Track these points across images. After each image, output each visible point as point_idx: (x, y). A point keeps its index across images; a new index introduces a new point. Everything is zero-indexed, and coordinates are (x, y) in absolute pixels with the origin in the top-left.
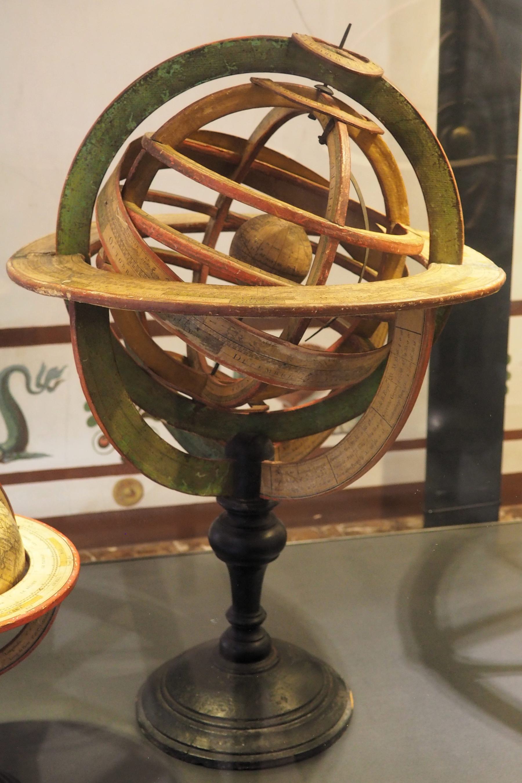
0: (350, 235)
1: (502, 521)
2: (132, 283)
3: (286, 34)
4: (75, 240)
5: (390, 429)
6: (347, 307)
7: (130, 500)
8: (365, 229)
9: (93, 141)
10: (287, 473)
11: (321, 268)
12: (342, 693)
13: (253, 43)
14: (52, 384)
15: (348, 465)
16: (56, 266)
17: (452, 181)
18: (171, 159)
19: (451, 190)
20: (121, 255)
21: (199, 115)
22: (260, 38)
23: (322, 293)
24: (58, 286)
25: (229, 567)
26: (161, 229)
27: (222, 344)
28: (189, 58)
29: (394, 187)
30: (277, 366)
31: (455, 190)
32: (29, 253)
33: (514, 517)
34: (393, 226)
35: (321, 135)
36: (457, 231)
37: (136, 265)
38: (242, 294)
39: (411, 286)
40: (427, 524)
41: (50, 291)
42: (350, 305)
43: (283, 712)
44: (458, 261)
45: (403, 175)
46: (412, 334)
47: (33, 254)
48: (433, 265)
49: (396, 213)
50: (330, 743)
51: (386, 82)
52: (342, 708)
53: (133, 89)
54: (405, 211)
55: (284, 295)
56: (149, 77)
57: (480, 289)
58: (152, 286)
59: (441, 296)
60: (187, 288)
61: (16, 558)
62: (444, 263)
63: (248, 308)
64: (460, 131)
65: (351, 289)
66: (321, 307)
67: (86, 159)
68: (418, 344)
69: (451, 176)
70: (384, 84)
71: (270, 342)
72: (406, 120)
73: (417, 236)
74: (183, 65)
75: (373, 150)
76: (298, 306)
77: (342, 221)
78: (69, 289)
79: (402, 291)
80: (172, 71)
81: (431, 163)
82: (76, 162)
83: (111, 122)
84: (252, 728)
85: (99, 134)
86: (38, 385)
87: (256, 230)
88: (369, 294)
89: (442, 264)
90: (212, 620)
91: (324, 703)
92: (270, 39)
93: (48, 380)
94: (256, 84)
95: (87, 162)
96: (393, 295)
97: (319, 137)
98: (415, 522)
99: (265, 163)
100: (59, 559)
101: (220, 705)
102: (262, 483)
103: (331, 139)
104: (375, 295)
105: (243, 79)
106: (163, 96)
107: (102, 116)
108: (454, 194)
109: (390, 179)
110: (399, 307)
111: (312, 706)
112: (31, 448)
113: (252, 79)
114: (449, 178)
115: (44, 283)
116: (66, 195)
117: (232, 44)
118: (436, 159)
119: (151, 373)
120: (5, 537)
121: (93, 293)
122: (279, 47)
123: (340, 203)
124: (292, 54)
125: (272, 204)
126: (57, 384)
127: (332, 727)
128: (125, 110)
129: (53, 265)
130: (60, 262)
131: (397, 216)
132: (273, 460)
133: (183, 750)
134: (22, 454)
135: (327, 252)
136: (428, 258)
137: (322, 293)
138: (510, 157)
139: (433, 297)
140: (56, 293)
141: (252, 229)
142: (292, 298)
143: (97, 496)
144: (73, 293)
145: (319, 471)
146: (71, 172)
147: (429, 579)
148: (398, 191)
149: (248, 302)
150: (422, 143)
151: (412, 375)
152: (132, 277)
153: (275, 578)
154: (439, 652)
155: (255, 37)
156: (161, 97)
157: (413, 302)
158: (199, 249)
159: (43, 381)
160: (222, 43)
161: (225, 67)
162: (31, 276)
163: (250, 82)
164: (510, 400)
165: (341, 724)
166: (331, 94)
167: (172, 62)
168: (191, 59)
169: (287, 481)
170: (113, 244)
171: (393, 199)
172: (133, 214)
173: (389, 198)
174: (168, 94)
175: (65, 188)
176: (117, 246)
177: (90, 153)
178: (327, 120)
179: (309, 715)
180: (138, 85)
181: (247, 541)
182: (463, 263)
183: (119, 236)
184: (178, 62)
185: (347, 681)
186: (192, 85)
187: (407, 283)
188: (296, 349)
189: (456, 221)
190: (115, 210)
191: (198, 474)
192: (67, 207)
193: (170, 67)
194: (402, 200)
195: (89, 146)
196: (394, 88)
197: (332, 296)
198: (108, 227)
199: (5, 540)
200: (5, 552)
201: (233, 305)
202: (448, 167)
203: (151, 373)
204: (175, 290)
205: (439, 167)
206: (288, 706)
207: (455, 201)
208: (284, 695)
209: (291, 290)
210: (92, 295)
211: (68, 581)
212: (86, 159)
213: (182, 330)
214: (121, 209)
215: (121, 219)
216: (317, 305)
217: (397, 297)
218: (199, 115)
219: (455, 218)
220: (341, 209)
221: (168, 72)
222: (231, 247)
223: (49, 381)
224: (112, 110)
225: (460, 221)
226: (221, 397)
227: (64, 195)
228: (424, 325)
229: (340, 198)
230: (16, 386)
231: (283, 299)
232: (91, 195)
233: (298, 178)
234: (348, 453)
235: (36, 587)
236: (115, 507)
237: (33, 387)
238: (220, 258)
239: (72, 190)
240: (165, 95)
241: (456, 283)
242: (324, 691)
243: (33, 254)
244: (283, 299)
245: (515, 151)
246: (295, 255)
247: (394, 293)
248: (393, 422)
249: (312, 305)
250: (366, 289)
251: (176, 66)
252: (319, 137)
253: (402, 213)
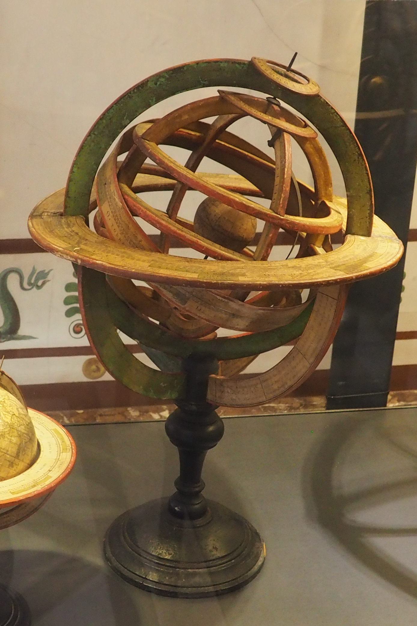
0: (288, 223)
1: (390, 405)
2: (124, 252)
3: (247, 58)
4: (78, 202)
5: (308, 366)
6: (284, 284)
7: (96, 374)
8: (299, 216)
9: (96, 133)
10: (228, 387)
11: (265, 247)
12: (258, 544)
13: (222, 65)
14: (40, 283)
15: (275, 387)
16: (66, 229)
17: (368, 174)
18: (157, 158)
19: (366, 180)
20: (116, 226)
21: (178, 120)
22: (227, 61)
23: (266, 269)
24: (71, 253)
25: (179, 451)
26: (148, 212)
27: (188, 299)
28: (172, 73)
29: (322, 173)
30: (228, 316)
31: (369, 181)
32: (43, 212)
33: (399, 401)
34: (320, 202)
35: (270, 139)
36: (369, 212)
37: (127, 236)
38: (207, 269)
39: (332, 264)
40: (329, 406)
41: (65, 256)
42: (286, 283)
43: (214, 558)
44: (368, 233)
45: (331, 170)
46: (330, 299)
47: (46, 214)
48: (349, 237)
49: (322, 192)
50: (246, 582)
51: (321, 97)
52: (257, 557)
54: (330, 191)
55: (238, 271)
56: (141, 87)
57: (382, 267)
58: (140, 257)
59: (353, 275)
60: (165, 260)
61: (33, 446)
62: (357, 235)
63: (212, 283)
64: (376, 80)
65: (287, 265)
66: (265, 284)
67: (90, 146)
68: (334, 307)
69: (367, 171)
70: (320, 100)
71: (224, 300)
72: (336, 127)
73: (338, 214)
74: (167, 79)
75: (308, 146)
76: (248, 282)
77: (282, 211)
78: (80, 257)
79: (325, 269)
80: (158, 83)
82: (82, 148)
83: (110, 119)
84: (191, 569)
85: (101, 127)
86: (30, 284)
87: (217, 206)
88: (300, 272)
89: (356, 236)
90: (176, 508)
91: (244, 552)
93: (37, 280)
94: (223, 98)
96: (318, 274)
97: (268, 141)
98: (319, 401)
99: (223, 143)
100: (61, 446)
101: (167, 550)
102: (209, 391)
103: (277, 144)
104: (305, 273)
105: (212, 92)
106: (150, 101)
107: (104, 114)
108: (368, 184)
109: (320, 167)
110: (322, 284)
111: (235, 554)
113: (219, 91)
114: (365, 172)
115: (61, 249)
116: (74, 172)
117: (205, 65)
119: (130, 306)
120: (26, 432)
121: (97, 262)
122: (241, 68)
123: (282, 199)
125: (232, 199)
126: (44, 283)
127: (249, 570)
129: (63, 228)
131: (323, 194)
132: (217, 374)
133: (138, 580)
134: (15, 336)
135: (271, 235)
136: (345, 229)
137: (266, 269)
139: (348, 276)
140: (69, 258)
141: (213, 204)
142: (244, 275)
143: (71, 370)
144: (82, 260)
145: (252, 389)
146: (78, 154)
148: (325, 176)
149: (212, 278)
150: (346, 145)
151: (328, 328)
152: (124, 246)
154: (333, 514)
155: (223, 59)
156: (149, 102)
157: (333, 280)
158: (176, 229)
159: (33, 281)
160: (197, 63)
161: (199, 82)
162: (49, 239)
163: (219, 95)
164: (403, 308)
165: (256, 568)
166: (279, 105)
167: (158, 76)
168: (173, 75)
169: (228, 392)
170: (110, 217)
171: (321, 183)
172: (126, 197)
173: (318, 182)
174: (154, 100)
175: (73, 167)
176: (113, 219)
177: (93, 141)
178: (275, 129)
179: (233, 561)
180: (132, 92)
181: (194, 433)
182: (372, 235)
183: (115, 212)
184: (163, 77)
185: (262, 535)
186: (173, 93)
187: (329, 260)
188: (243, 305)
189: (368, 204)
190: (112, 191)
191: (162, 384)
193: (158, 80)
194: (328, 183)
195: (93, 136)
196: (327, 103)
197: (273, 273)
198: (106, 202)
199: (26, 434)
200: (26, 443)
201: (201, 280)
202: (365, 164)
203: (130, 306)
204: (157, 262)
206: (219, 554)
207: (368, 189)
208: (215, 545)
209: (243, 265)
210: (97, 264)
211: (69, 465)
212: (90, 146)
213: (159, 286)
214: (118, 193)
215: (117, 200)
216: (262, 283)
217: (321, 276)
218: (178, 120)
220: (283, 204)
221: (156, 84)
222: (195, 216)
223: (38, 280)
224: (112, 111)
225: (372, 204)
226: (183, 329)
227: (72, 172)
228: (340, 293)
229: (282, 195)
230: (13, 284)
231: (238, 275)
232: (93, 172)
233: (248, 156)
234: (276, 379)
235: (47, 468)
237: (26, 285)
238: (191, 237)
241: (365, 260)
242: (245, 544)
243: (46, 214)
244: (238, 275)
246: (245, 227)
247: (319, 271)
248: (312, 360)
249: (258, 283)
250: (298, 266)
251: (163, 80)
252: (268, 141)
253: (327, 192)
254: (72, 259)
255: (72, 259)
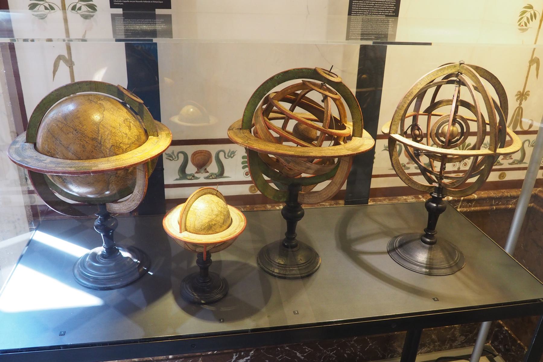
1: (369, 204)
3: (313, 67)
22: (306, 69)
25: (287, 222)
44: (361, 136)
48: (353, 138)
50: (313, 273)
52: (317, 263)
53: (267, 82)
64: (364, 76)
73: (349, 129)
75: (337, 102)
77: (327, 128)
82: (248, 103)
86: (228, 156)
92: (308, 69)
93: (231, 155)
94: (304, 83)
103: (325, 101)
105: (299, 81)
112: (225, 174)
130: (243, 133)
137: (321, 150)
138: (379, 88)
142: (312, 153)
143: (245, 190)
146: (247, 105)
147: (344, 224)
153: (301, 224)
160: (294, 69)
165: (317, 267)
167: (279, 74)
171: (342, 116)
181: (292, 214)
194: (345, 116)
206: (302, 262)
208: (301, 258)
219: (361, 123)
227: (245, 112)
236: (250, 193)
245: (382, 86)
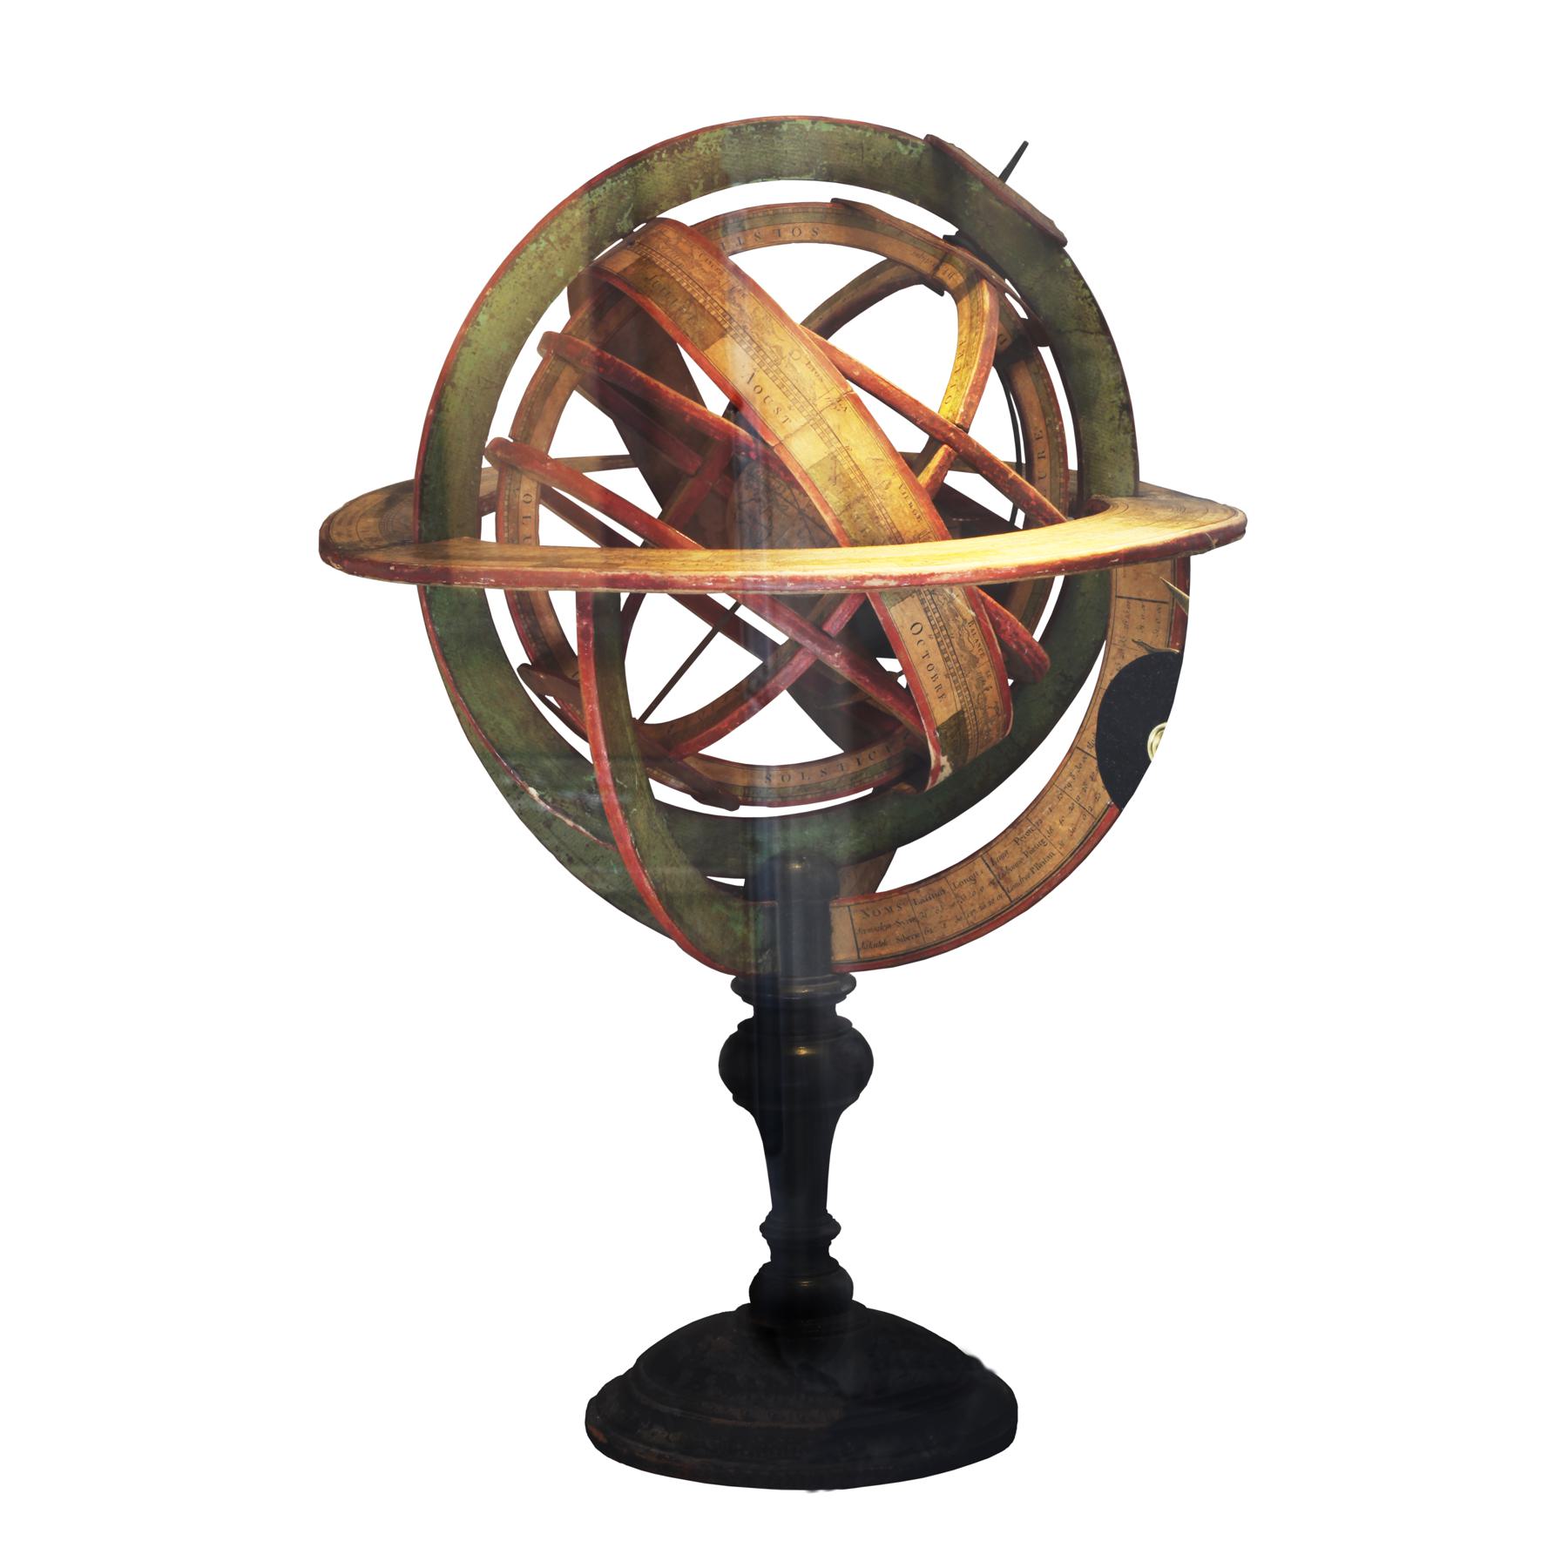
9: (552, 238)
15: (1064, 829)
20: (936, 658)
81: (1107, 417)
95: (531, 272)
105: (824, 192)
118: (1116, 411)
124: (939, 171)
128: (622, 197)
174: (701, 187)
177: (541, 257)
192: (474, 345)
195: (544, 243)
205: (858, 500)
239: (492, 316)
240: (696, 186)
254: (780, 969)
255: (780, 969)
